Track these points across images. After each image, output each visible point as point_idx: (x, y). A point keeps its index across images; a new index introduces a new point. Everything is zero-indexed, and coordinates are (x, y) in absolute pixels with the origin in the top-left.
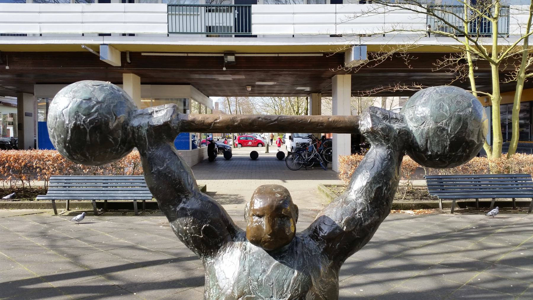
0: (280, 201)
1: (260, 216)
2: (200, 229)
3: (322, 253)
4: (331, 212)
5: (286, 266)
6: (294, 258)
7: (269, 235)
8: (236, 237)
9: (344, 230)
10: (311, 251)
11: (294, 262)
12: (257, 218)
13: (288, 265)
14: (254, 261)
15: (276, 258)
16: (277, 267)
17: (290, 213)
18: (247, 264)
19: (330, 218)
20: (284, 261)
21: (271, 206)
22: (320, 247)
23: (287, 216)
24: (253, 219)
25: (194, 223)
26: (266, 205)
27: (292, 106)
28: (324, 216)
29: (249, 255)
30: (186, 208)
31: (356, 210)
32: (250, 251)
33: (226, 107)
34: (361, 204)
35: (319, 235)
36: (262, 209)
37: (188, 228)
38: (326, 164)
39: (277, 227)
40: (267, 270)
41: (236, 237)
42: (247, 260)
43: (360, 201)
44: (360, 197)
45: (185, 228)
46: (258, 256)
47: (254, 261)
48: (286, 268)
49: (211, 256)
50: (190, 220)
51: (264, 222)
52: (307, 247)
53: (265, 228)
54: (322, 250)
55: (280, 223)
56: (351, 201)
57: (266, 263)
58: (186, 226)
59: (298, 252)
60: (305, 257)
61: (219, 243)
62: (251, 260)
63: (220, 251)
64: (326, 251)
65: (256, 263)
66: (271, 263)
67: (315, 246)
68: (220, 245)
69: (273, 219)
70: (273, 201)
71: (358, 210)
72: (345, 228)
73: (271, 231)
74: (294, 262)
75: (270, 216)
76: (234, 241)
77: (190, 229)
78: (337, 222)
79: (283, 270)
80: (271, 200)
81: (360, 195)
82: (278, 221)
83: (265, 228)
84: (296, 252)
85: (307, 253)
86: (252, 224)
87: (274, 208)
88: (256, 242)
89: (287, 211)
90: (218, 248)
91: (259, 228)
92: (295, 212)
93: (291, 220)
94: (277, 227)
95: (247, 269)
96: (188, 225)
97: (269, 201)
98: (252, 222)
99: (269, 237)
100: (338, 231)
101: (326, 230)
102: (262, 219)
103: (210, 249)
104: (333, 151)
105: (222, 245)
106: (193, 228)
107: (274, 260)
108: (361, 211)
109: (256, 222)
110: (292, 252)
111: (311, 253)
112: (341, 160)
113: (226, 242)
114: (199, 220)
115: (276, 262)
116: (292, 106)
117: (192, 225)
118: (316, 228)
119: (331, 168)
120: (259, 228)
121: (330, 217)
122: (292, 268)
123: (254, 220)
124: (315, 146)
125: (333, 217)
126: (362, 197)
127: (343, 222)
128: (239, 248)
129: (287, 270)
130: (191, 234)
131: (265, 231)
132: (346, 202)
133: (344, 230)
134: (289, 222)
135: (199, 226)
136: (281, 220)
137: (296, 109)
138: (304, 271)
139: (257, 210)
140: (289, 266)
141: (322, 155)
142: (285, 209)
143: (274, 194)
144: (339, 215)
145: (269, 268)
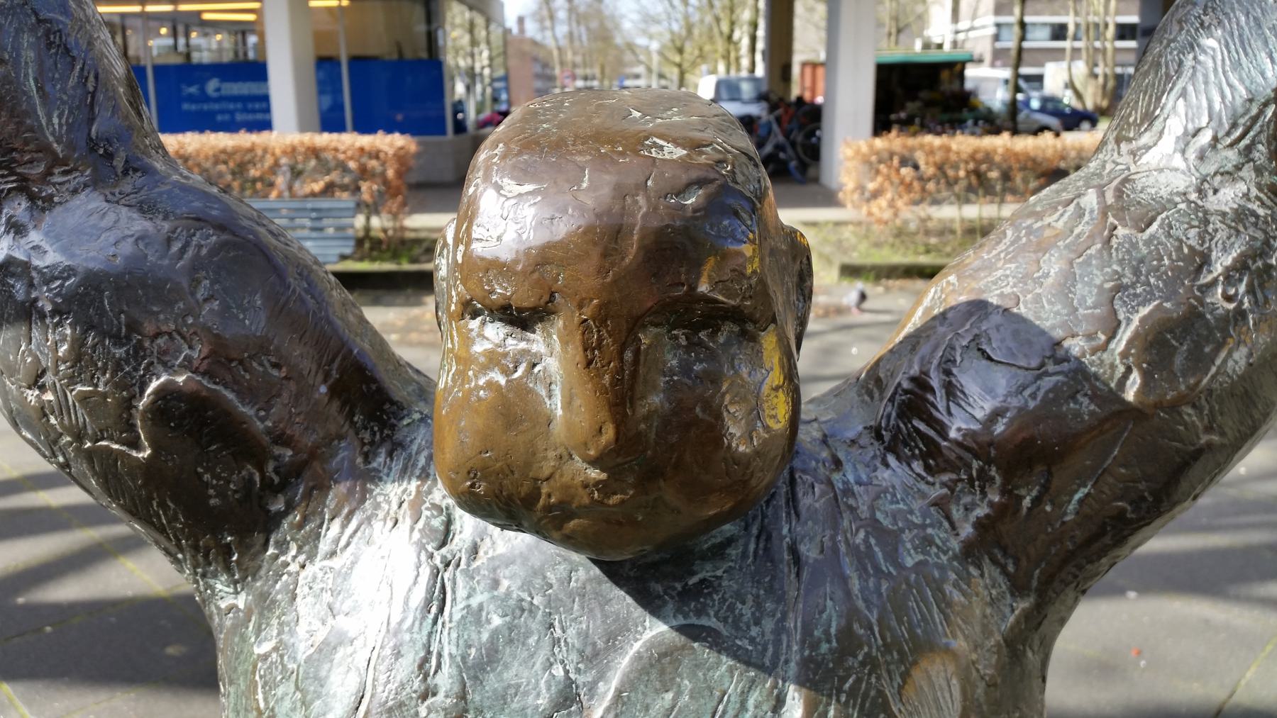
0: (682, 192)
1: (520, 318)
2: (128, 405)
3: (970, 552)
4: (1025, 278)
5: (727, 662)
6: (780, 599)
7: (594, 463)
8: (397, 446)
9: (1130, 395)
10: (890, 540)
11: (780, 630)
12: (495, 332)
13: (735, 654)
14: (497, 621)
15: (650, 603)
16: (658, 667)
17: (761, 292)
18: (448, 645)
19: (1020, 319)
20: (711, 622)
21: (607, 236)
22: (957, 513)
23: (736, 315)
24: (467, 341)
25: (80, 361)
26: (562, 229)
27: (718, 20)
28: (979, 308)
29: (470, 576)
30: (26, 266)
31: (1206, 260)
32: (474, 550)
33: (543, 29)
34: (1241, 216)
35: (942, 430)
36: (543, 259)
37: (49, 396)
38: (803, 167)
39: (656, 400)
40: (592, 687)
41: (397, 446)
42: (454, 611)
43: (1228, 197)
44: (1230, 175)
45: (32, 395)
46: (527, 585)
47: (497, 621)
48: (725, 673)
49: (228, 569)
50: (53, 343)
51: (551, 354)
52: (864, 511)
53: (556, 405)
54: (967, 530)
55: (686, 369)
56: (1165, 205)
57: (584, 636)
58: (36, 381)
59: (809, 551)
60: (855, 584)
61: (272, 489)
62: (475, 616)
63: (283, 547)
64: (988, 542)
65: (512, 635)
66: (615, 636)
67: (917, 505)
68: (278, 505)
69: (628, 338)
70: (621, 193)
71: (1222, 262)
72: (1135, 380)
73: (609, 433)
74: (780, 630)
75: (602, 317)
76: (374, 477)
77: (62, 407)
78: (1076, 346)
79: (704, 690)
80: (609, 179)
81: (1232, 156)
82: (666, 352)
83: (556, 405)
84: (794, 550)
85: (863, 557)
86: (461, 376)
87: (632, 250)
88: (506, 497)
89: (740, 274)
90: (270, 523)
91: (514, 409)
92: (791, 281)
93: (769, 341)
94: (656, 400)
95: (445, 680)
96: (49, 379)
97: (591, 191)
98: (465, 361)
99: (595, 474)
100: (1086, 406)
101: (981, 402)
102: (536, 342)
103: (216, 531)
104: (824, 133)
105: (290, 507)
106: (84, 398)
107: (638, 612)
108: (1241, 266)
109: (494, 359)
110: (767, 555)
111: (893, 557)
112: (849, 152)
113: (321, 487)
114: (118, 340)
115: (655, 630)
116: (718, 20)
117: (72, 380)
118: (921, 383)
119: (816, 180)
120: (514, 409)
121: (1022, 310)
122: (768, 670)
123: (479, 348)
124: (778, 120)
125: (1046, 314)
126: (1247, 172)
127: (1120, 344)
128: (405, 524)
129: (733, 689)
130: (79, 437)
131: (558, 428)
132: (1127, 204)
133: (1130, 395)
134: (756, 360)
135: (120, 386)
136: (693, 345)
137: (725, 27)
138: (852, 693)
139: (495, 267)
140: (746, 660)
141: (793, 144)
142: (725, 256)
143: (636, 143)
144: (1088, 295)
145: (601, 676)
